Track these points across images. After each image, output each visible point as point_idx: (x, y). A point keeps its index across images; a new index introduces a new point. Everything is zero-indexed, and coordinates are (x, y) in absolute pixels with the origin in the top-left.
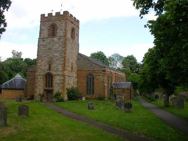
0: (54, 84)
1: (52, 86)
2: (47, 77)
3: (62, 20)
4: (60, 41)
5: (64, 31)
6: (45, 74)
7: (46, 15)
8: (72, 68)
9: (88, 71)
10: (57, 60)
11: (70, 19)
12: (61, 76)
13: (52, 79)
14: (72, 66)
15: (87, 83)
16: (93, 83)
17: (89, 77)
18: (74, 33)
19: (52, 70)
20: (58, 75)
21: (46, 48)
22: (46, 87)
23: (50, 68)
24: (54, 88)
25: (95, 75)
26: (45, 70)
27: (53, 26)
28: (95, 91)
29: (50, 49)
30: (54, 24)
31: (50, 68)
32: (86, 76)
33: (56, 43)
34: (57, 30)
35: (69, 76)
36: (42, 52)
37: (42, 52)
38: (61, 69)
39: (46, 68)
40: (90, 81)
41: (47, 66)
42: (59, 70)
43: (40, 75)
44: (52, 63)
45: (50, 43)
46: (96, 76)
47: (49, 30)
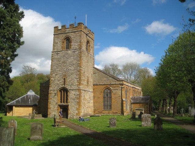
1: (67, 102)
14: (88, 80)
15: (104, 97)
16: (111, 97)
19: (67, 84)
22: (61, 102)
24: (69, 104)
25: (112, 89)
29: (64, 62)
40: (107, 95)
41: (62, 80)
44: (67, 77)
46: (113, 90)
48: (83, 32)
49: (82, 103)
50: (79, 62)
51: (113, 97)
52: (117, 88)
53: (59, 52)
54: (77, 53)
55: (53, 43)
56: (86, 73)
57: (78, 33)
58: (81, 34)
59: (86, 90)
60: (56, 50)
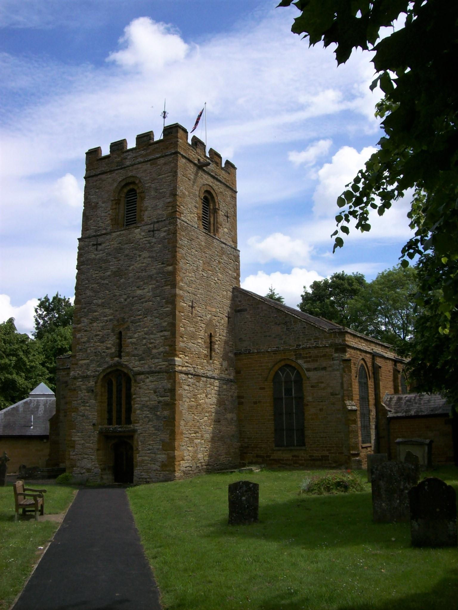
0: (138, 412)
1: (129, 421)
2: (110, 384)
3: (162, 161)
4: (154, 240)
5: (168, 200)
6: (104, 370)
7: (106, 151)
8: (211, 343)
9: (275, 352)
10: (147, 312)
11: (193, 155)
12: (161, 375)
13: (129, 389)
14: (211, 336)
15: (277, 400)
16: (300, 399)
17: (283, 377)
18: (216, 211)
19: (128, 354)
20: (152, 373)
21: (106, 270)
22: (110, 422)
23: (120, 346)
24: (138, 427)
25: (305, 366)
26: (102, 358)
27: (131, 187)
28: (308, 433)
29: (119, 273)
30: (132, 180)
31: (120, 346)
32: (273, 373)
33: (143, 249)
34: (143, 199)
35: (197, 376)
36: (92, 289)
37: (92, 289)
38: (162, 349)
39: (108, 348)
40: (288, 391)
41: (112, 340)
42: (154, 351)
43: (87, 377)
44: (128, 328)
45: (119, 250)
46: (309, 370)
47: (118, 202)
48: (183, 157)
49: (182, 423)
50: (170, 268)
51: (309, 398)
52: (324, 364)
53: (100, 240)
54: (163, 234)
55: (82, 208)
56: (198, 310)
57: (165, 164)
58: (176, 166)
59: (201, 372)
60: (91, 232)
